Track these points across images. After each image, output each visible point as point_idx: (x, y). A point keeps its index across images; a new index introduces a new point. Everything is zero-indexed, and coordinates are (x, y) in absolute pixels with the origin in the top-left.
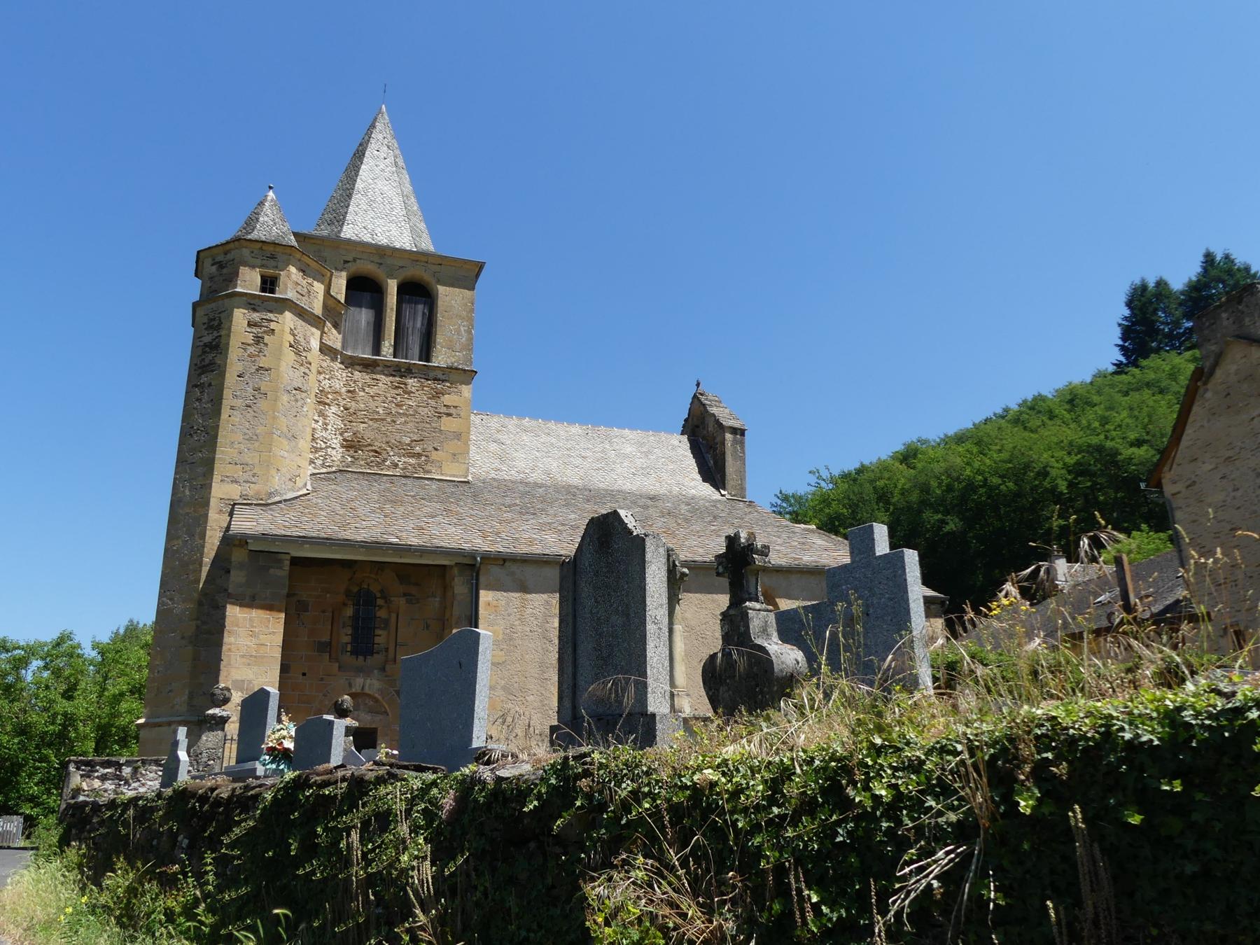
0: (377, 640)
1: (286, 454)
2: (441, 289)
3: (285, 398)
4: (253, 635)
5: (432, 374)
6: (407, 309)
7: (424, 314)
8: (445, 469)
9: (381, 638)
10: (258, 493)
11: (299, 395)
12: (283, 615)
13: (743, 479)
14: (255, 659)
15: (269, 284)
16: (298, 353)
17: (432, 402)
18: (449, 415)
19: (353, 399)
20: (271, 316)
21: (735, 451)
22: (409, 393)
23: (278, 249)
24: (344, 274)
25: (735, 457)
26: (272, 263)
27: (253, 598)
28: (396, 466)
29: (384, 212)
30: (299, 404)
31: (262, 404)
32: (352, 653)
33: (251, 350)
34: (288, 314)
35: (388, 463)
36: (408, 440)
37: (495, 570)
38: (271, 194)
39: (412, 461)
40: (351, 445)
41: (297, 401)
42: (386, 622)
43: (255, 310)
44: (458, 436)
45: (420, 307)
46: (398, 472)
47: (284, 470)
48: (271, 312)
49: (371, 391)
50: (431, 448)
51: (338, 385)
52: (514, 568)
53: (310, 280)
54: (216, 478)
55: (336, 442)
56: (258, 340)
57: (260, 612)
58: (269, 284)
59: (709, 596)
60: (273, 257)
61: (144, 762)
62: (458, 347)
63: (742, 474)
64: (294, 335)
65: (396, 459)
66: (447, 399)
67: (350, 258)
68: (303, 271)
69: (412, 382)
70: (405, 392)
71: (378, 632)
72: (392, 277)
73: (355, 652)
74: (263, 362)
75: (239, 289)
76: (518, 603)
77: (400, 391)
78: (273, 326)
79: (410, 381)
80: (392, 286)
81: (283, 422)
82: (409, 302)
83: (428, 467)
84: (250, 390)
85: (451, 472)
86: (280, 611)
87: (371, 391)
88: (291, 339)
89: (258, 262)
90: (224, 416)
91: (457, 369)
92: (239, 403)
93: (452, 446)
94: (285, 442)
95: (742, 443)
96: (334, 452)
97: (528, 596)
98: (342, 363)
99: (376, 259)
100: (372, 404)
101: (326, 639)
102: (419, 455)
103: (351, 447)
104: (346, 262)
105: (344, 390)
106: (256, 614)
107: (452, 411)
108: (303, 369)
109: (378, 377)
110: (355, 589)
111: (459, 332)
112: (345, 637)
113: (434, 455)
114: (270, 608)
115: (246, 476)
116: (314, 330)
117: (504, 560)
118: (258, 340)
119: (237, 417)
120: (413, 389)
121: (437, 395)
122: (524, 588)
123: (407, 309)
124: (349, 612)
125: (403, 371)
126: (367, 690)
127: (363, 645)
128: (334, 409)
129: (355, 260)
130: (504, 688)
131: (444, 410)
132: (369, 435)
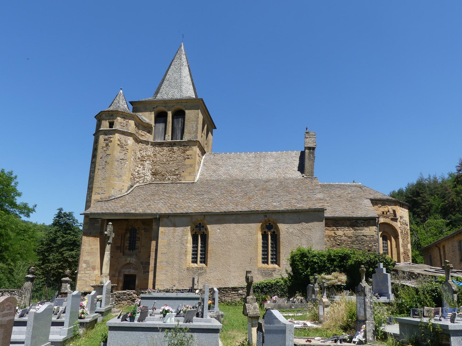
0: (136, 245)
1: (117, 182)
2: (187, 112)
3: (116, 163)
4: (90, 246)
5: (183, 144)
6: (175, 120)
7: (182, 122)
8: (187, 179)
9: (138, 244)
10: (106, 197)
11: (122, 161)
12: (99, 239)
13: (313, 168)
14: (90, 254)
15: (111, 125)
16: (122, 147)
17: (182, 155)
18: (188, 158)
19: (155, 157)
20: (111, 136)
21: (310, 156)
22: (174, 152)
23: (114, 112)
24: (153, 113)
25: (310, 159)
26: (112, 117)
27: (90, 234)
28: (169, 179)
29: (181, 85)
30: (123, 164)
31: (108, 167)
32: (129, 249)
33: (105, 149)
34: (117, 135)
35: (167, 179)
36: (173, 170)
37: (165, 220)
38: (121, 91)
39: (175, 177)
40: (154, 174)
41: (122, 163)
42: (139, 238)
43: (106, 135)
44: (191, 166)
45: (180, 119)
46: (170, 182)
47: (116, 188)
48: (111, 134)
49: (161, 154)
50: (181, 172)
51: (149, 153)
52: (171, 218)
53: (127, 120)
54: (93, 193)
55: (149, 174)
56: (107, 145)
57: (92, 238)
58: (111, 125)
59: (248, 224)
60: (112, 115)
61: (5, 291)
62: (192, 132)
63: (312, 167)
64: (120, 141)
65: (169, 177)
66: (188, 153)
67: (155, 106)
68: (124, 118)
69: (175, 148)
70: (173, 152)
71: (137, 242)
72: (169, 110)
73: (130, 249)
74: (108, 152)
75: (101, 129)
76: (172, 231)
77: (171, 152)
78: (111, 139)
79: (175, 148)
80: (170, 114)
81: (115, 172)
82: (176, 118)
83: (180, 179)
84: (104, 162)
85: (188, 179)
86: (98, 237)
87: (161, 154)
88: (119, 143)
89: (108, 118)
90: (96, 172)
91: (191, 141)
92: (101, 167)
93: (189, 170)
94: (116, 178)
95: (313, 153)
96: (148, 177)
97: (177, 228)
98: (151, 145)
99: (164, 105)
100: (162, 158)
101: (119, 245)
102: (177, 174)
103: (154, 174)
104: (154, 108)
105: (152, 154)
106: (91, 239)
107: (190, 157)
108: (124, 152)
109: (164, 148)
110: (130, 228)
111: (193, 127)
112: (127, 245)
113: (183, 174)
114: (95, 236)
115: (102, 192)
116: (129, 137)
117: (169, 216)
118: (107, 145)
119: (100, 172)
120: (176, 151)
121: (184, 152)
122: (175, 226)
123: (175, 120)
124: (128, 235)
125: (171, 145)
126: (131, 262)
127: (132, 247)
128: (147, 162)
129: (157, 107)
130: (166, 262)
131: (187, 157)
132: (160, 169)
